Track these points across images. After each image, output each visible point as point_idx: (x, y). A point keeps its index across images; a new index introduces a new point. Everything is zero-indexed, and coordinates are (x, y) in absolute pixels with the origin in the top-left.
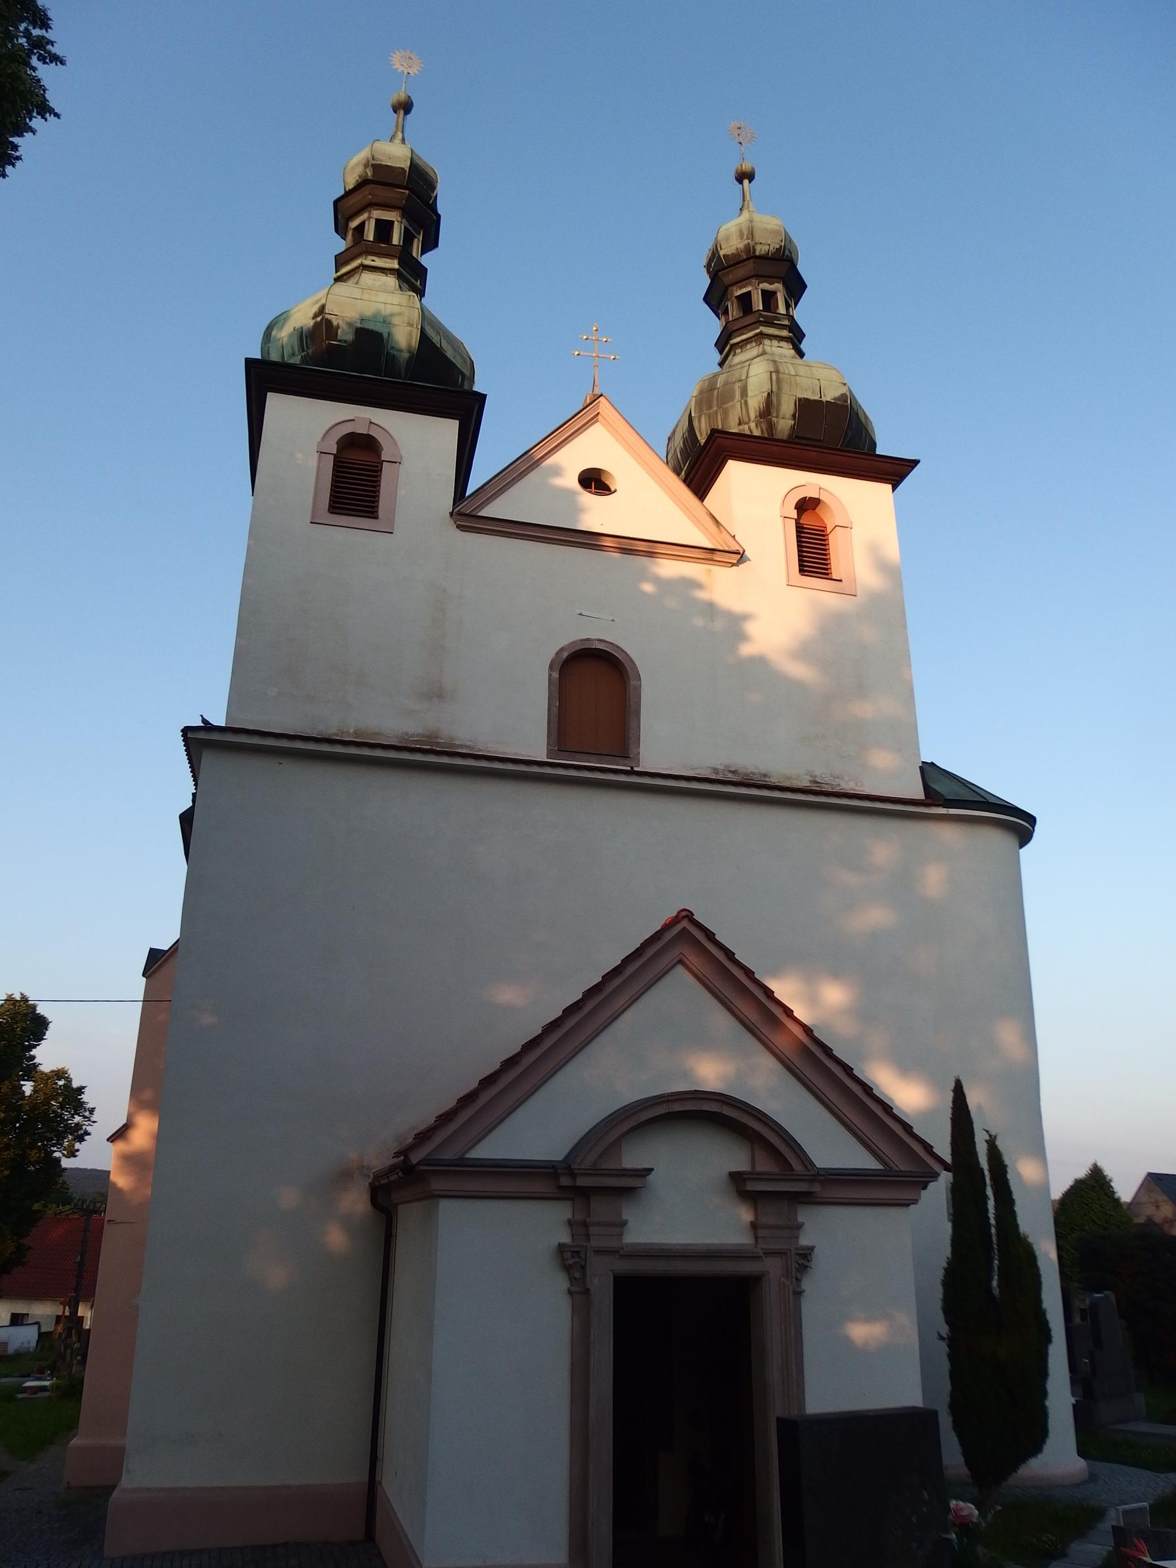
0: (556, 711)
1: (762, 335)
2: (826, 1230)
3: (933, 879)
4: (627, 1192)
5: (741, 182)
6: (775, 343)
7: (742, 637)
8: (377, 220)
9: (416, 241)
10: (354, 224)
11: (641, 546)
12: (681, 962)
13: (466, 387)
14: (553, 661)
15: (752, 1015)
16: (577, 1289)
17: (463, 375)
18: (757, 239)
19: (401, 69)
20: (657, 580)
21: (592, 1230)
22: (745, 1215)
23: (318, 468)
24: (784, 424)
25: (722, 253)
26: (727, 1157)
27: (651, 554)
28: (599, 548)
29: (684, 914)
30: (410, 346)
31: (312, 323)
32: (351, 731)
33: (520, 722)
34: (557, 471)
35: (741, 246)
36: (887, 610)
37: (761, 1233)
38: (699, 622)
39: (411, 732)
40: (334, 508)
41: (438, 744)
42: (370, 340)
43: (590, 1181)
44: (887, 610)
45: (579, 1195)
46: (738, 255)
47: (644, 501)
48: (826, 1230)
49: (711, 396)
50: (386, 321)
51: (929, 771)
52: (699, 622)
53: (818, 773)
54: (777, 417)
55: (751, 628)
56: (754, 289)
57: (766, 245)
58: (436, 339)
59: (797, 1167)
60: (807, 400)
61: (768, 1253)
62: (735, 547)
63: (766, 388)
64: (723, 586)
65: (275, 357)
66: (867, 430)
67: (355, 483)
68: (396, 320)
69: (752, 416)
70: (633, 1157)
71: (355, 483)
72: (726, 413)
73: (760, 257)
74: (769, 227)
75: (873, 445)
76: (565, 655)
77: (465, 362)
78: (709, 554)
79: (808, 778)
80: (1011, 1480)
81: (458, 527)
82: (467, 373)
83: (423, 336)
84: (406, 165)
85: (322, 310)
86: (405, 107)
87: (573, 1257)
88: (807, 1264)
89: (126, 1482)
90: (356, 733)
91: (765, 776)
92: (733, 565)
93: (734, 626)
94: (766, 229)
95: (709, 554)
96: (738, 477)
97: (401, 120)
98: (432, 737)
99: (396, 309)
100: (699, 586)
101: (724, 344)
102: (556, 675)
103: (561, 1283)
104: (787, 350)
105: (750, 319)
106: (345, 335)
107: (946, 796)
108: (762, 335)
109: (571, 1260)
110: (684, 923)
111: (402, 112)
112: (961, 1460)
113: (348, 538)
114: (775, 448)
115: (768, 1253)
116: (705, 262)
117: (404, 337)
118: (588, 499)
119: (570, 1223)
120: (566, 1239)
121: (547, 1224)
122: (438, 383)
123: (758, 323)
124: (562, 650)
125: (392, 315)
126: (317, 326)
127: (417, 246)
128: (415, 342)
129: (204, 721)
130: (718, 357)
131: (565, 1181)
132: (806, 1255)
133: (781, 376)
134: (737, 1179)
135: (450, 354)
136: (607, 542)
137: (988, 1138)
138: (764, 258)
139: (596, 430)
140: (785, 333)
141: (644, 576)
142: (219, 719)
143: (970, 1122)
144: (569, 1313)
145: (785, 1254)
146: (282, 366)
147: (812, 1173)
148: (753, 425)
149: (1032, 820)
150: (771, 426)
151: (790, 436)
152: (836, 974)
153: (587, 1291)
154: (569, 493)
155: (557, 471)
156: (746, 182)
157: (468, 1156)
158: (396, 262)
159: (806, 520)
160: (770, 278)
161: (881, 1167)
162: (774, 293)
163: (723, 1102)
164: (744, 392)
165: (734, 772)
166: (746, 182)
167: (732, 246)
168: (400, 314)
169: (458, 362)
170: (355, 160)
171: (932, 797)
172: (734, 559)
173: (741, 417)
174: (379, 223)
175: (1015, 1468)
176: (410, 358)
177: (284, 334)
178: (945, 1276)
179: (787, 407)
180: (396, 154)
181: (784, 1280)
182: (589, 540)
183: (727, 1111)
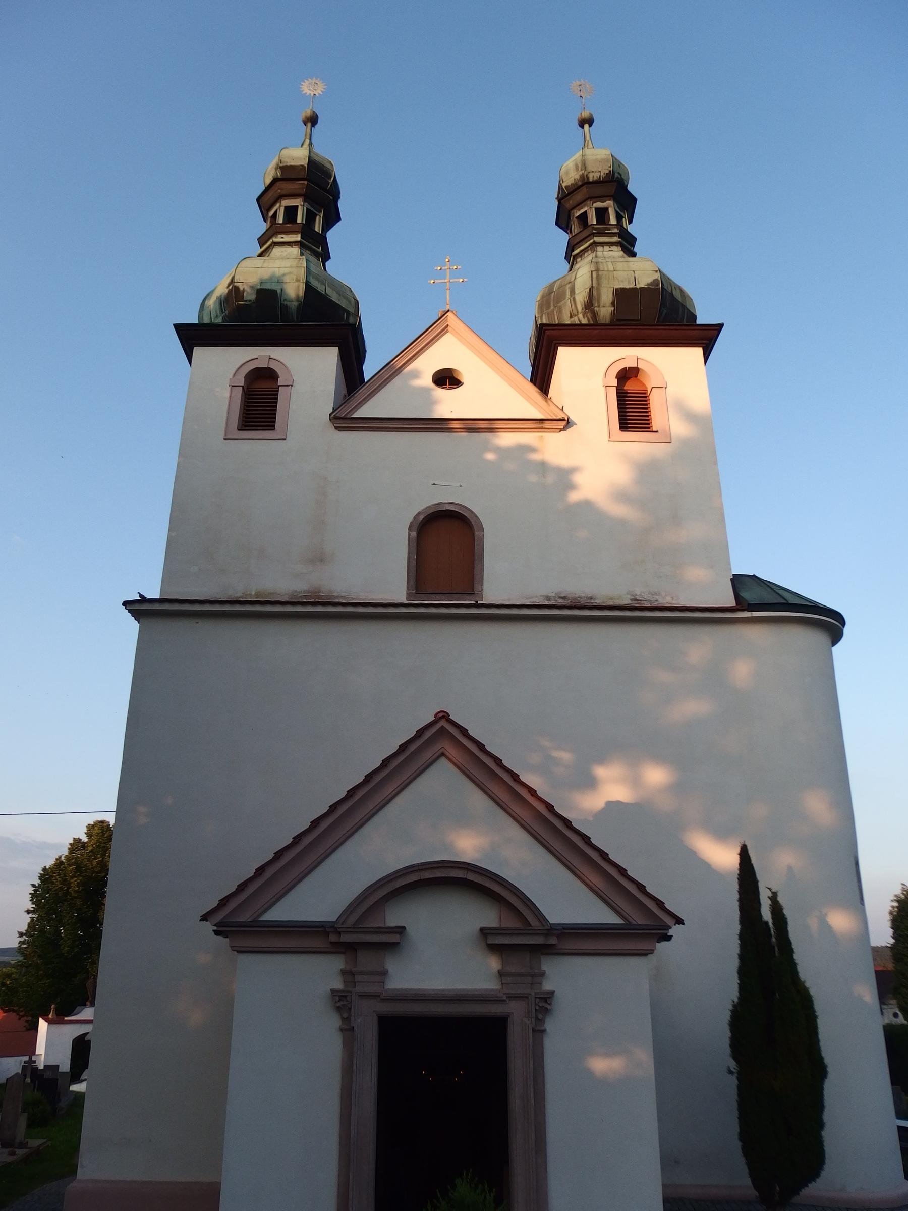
0: (414, 562)
1: (596, 244)
2: (564, 976)
3: (742, 671)
4: (391, 947)
5: (582, 127)
6: (607, 248)
7: (571, 487)
8: (285, 207)
9: (318, 218)
10: (271, 213)
11: (483, 425)
12: (443, 754)
13: (351, 320)
14: (411, 523)
15: (504, 796)
16: (346, 1027)
17: (348, 313)
18: (590, 168)
19: (308, 92)
20: (498, 450)
22: (494, 963)
23: (230, 396)
24: (605, 311)
25: (564, 185)
26: (472, 916)
27: (492, 430)
28: (450, 430)
29: (441, 715)
30: (298, 296)
31: (226, 291)
32: (253, 593)
33: (386, 575)
34: (416, 375)
35: (577, 177)
36: (701, 453)
38: (533, 478)
39: (298, 590)
40: (246, 426)
42: (268, 296)
43: (360, 938)
44: (701, 453)
45: (349, 949)
46: (576, 184)
47: (491, 388)
48: (564, 976)
49: (551, 298)
50: (279, 281)
51: (738, 581)
52: (533, 478)
53: (638, 593)
54: (599, 306)
55: (578, 479)
56: (597, 207)
57: (597, 172)
58: (320, 288)
59: (534, 923)
60: (623, 290)
61: (512, 997)
62: (561, 416)
63: (589, 284)
64: (553, 448)
65: (206, 320)
66: (684, 307)
67: (259, 405)
68: (287, 279)
69: (580, 309)
70: (394, 917)
71: (259, 405)
72: (560, 310)
73: (594, 182)
74: (599, 157)
75: (694, 317)
76: (421, 517)
77: (350, 302)
78: (539, 424)
79: (629, 597)
80: (796, 1200)
81: (336, 428)
82: (351, 310)
83: (308, 286)
84: (305, 162)
85: (232, 281)
86: (312, 120)
88: (549, 1007)
89: (80, 1174)
90: (257, 595)
91: (591, 598)
92: (561, 430)
93: (564, 478)
94: (596, 159)
95: (539, 424)
96: (570, 360)
97: (309, 130)
99: (287, 270)
100: (532, 449)
101: (571, 257)
102: (414, 534)
103: (335, 1021)
104: (617, 252)
105: (586, 232)
106: (250, 296)
107: (759, 601)
108: (596, 244)
109: (341, 1002)
110: (443, 723)
111: (309, 125)
112: (748, 1182)
113: (256, 448)
114: (595, 332)
115: (512, 997)
116: (257, 196)
117: (293, 289)
118: (440, 392)
119: (343, 972)
120: (338, 985)
121: (324, 973)
122: (327, 320)
123: (594, 235)
124: (419, 514)
125: (284, 275)
126: (230, 292)
127: (625, 222)
128: (301, 293)
129: (141, 596)
130: (568, 266)
131: (333, 938)
132: (547, 998)
133: (600, 273)
134: (484, 932)
135: (334, 297)
136: (455, 425)
137: (770, 894)
138: (597, 182)
139: (447, 338)
140: (615, 239)
141: (488, 448)
142: (153, 593)
143: (755, 882)
144: (341, 1046)
145: (527, 997)
146: (211, 326)
147: (546, 928)
148: (581, 316)
149: (839, 618)
150: (594, 315)
151: (612, 320)
152: (659, 758)
154: (425, 390)
155: (416, 375)
156: (586, 126)
157: (262, 919)
158: (299, 236)
159: (629, 386)
160: (602, 198)
161: (623, 922)
162: (606, 209)
163: (468, 870)
164: (573, 291)
165: (564, 598)
166: (586, 126)
167: (572, 177)
168: (290, 273)
170: (270, 167)
171: (741, 604)
172: (561, 425)
173: (572, 312)
174: (287, 208)
175: (796, 1191)
176: (299, 307)
177: (211, 302)
178: (732, 1017)
179: (606, 297)
180: (298, 156)
181: (526, 1020)
182: (440, 425)
183: (471, 877)
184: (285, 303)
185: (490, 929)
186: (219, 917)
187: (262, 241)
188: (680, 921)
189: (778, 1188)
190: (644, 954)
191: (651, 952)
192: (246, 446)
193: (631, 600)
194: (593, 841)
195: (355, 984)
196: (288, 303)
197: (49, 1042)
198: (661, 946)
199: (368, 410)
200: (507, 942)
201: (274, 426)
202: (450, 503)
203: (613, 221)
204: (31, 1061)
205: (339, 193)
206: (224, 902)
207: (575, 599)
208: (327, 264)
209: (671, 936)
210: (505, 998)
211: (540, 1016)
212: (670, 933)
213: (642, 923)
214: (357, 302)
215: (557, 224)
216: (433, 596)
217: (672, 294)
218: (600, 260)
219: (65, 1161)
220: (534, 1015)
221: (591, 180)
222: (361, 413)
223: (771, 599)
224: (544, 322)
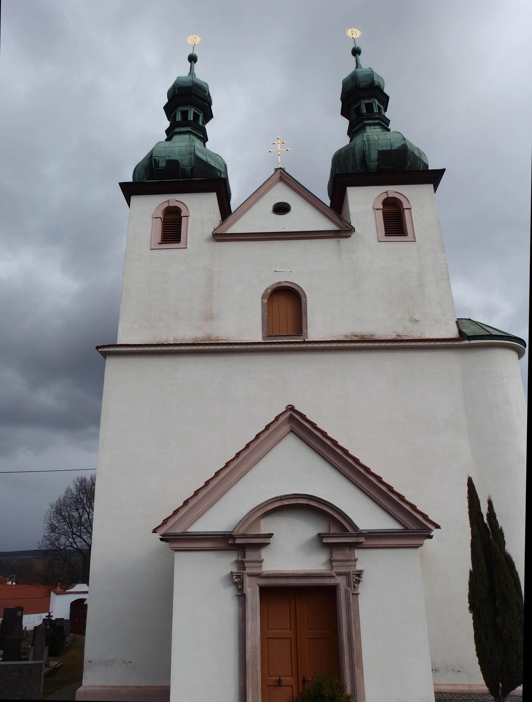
6: (372, 127)
10: (172, 116)
13: (223, 176)
17: (221, 172)
21: (246, 565)
29: (290, 407)
33: (250, 326)
37: (334, 564)
39: (198, 337)
41: (211, 340)
43: (240, 544)
45: (242, 548)
48: (369, 562)
58: (204, 158)
60: (384, 151)
61: (339, 574)
66: (420, 160)
67: (171, 229)
69: (358, 163)
71: (171, 229)
75: (427, 166)
76: (269, 291)
77: (221, 166)
79: (395, 334)
82: (222, 170)
87: (236, 578)
89: (86, 682)
91: (372, 336)
98: (209, 338)
102: (265, 301)
109: (237, 582)
112: (483, 682)
113: (171, 254)
115: (339, 574)
120: (235, 570)
121: (224, 564)
124: (267, 289)
132: (359, 574)
135: (212, 163)
148: (359, 168)
153: (244, 595)
157: (187, 531)
160: (369, 97)
165: (356, 336)
169: (217, 166)
171: (462, 336)
184: (183, 167)
185: (324, 534)
186: (163, 531)
187: (168, 132)
188: (438, 527)
189: (10, 583)
190: (417, 547)
191: (421, 545)
192: (163, 253)
193: (396, 336)
194: (384, 480)
195: (244, 568)
196: (185, 168)
197: (60, 607)
198: (427, 541)
199: (236, 228)
200: (349, 541)
201: (180, 240)
202: (285, 282)
203: (376, 110)
204: (49, 616)
205: (211, 102)
206: (165, 522)
207: (362, 336)
208: (206, 144)
209: (432, 536)
210: (335, 575)
211: (356, 585)
212: (432, 534)
213: (414, 528)
214: (226, 165)
215: (341, 114)
216: (278, 337)
217: (413, 153)
218: (369, 134)
219: (75, 674)
220: (352, 585)
221: (361, 87)
222: (230, 231)
223: (480, 332)
224: (337, 172)
